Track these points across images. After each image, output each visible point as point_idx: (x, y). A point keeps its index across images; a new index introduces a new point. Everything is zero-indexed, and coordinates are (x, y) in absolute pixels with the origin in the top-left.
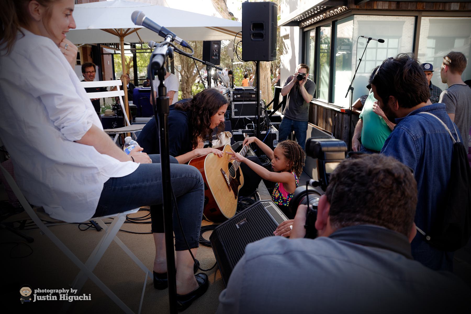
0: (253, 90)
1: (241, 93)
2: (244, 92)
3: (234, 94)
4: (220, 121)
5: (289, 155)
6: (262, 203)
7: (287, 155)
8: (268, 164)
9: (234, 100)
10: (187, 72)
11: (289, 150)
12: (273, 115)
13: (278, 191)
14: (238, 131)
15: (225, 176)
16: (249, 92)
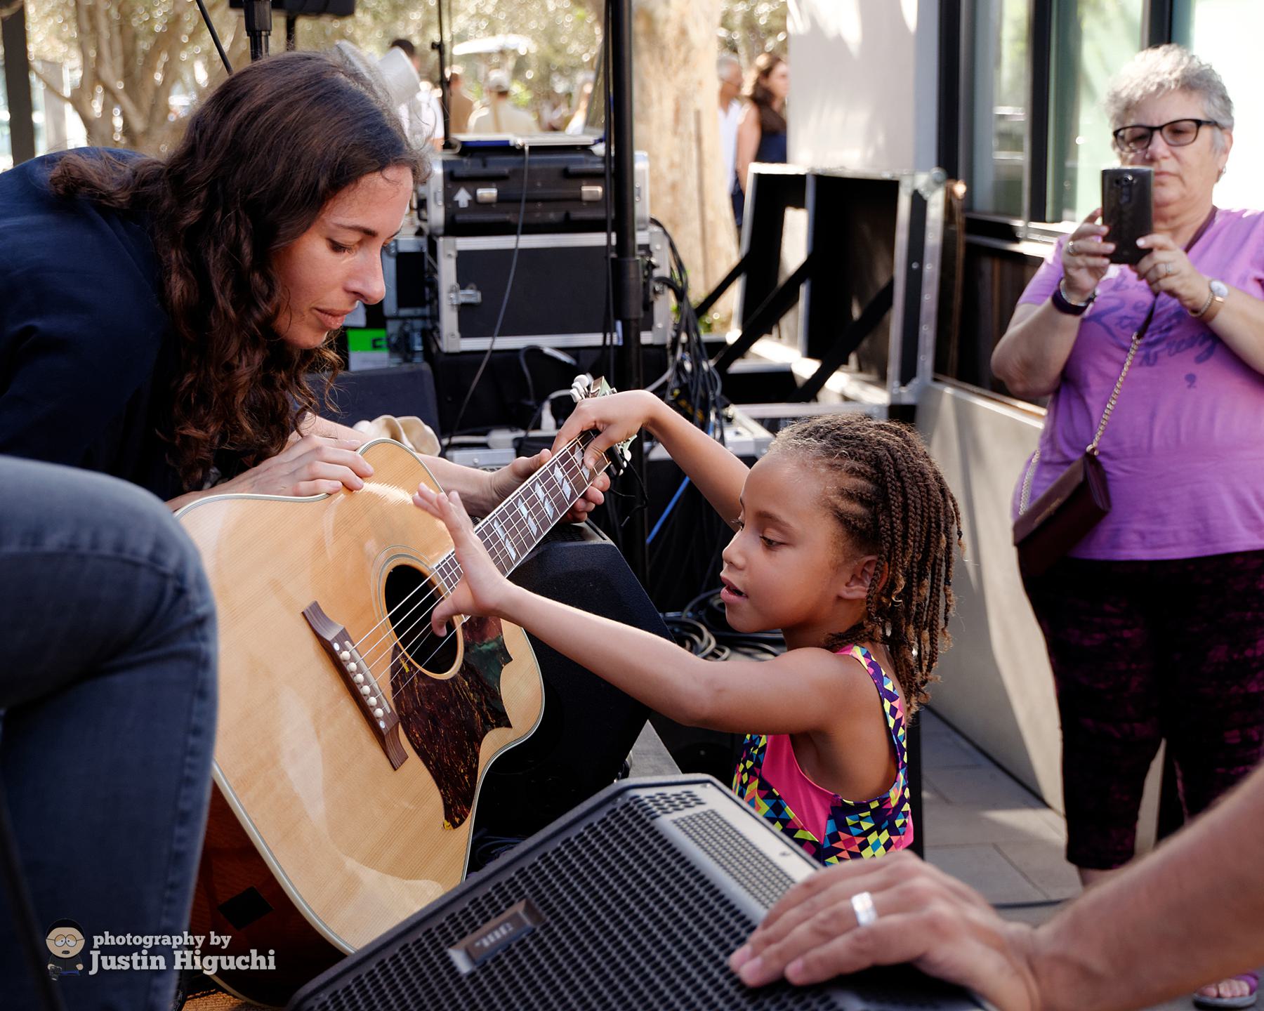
0: (585, 149)
1: (506, 170)
2: (523, 161)
3: (453, 179)
6: (643, 793)
9: (454, 227)
10: (124, 99)
12: (738, 366)
13: (756, 784)
14: (485, 446)
15: (345, 655)
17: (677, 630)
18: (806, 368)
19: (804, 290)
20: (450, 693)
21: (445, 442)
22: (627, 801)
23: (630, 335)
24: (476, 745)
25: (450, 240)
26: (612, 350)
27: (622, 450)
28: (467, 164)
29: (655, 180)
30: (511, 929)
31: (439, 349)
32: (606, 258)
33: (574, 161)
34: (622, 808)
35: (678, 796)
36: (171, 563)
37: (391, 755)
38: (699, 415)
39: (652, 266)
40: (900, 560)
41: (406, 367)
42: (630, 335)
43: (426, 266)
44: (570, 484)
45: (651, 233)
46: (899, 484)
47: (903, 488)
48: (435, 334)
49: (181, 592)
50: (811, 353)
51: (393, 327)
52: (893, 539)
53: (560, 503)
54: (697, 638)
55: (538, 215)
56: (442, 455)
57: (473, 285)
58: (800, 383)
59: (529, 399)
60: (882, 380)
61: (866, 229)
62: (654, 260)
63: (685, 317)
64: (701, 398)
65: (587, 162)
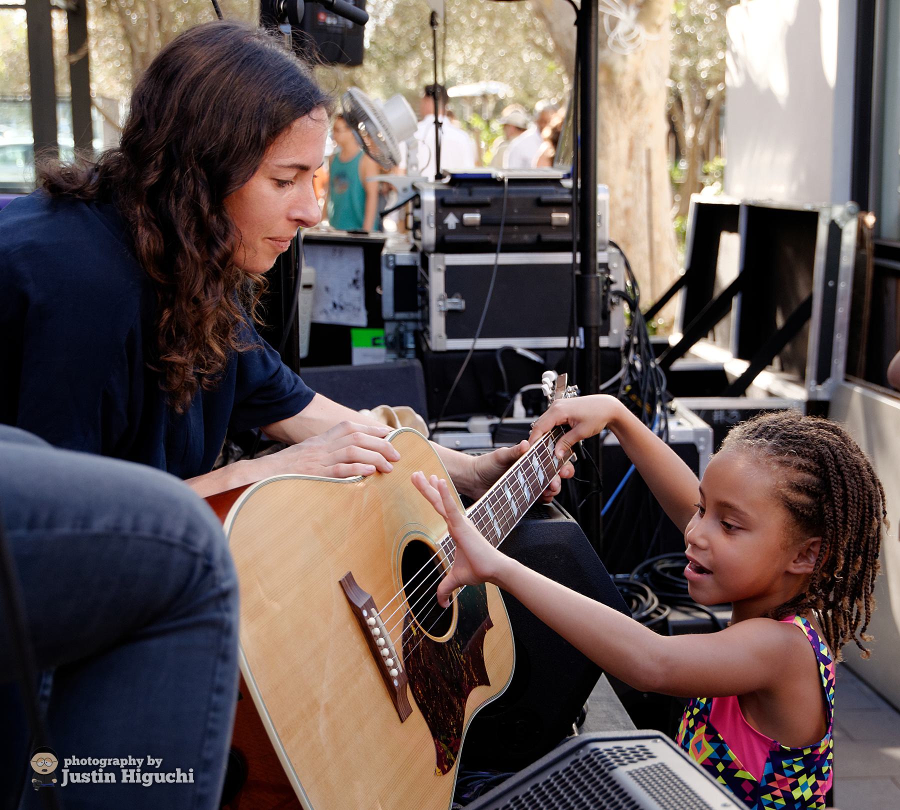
0: (556, 182)
1: (488, 199)
2: (503, 192)
3: (443, 205)
6: (602, 746)
9: (444, 245)
12: (679, 365)
13: (703, 729)
14: (465, 430)
15: (371, 621)
16: (532, 191)
17: (625, 590)
18: (737, 368)
19: (736, 302)
21: (432, 426)
23: (591, 339)
25: (440, 256)
26: (575, 352)
29: (612, 206)
31: (428, 347)
32: (572, 274)
33: (546, 192)
36: (201, 543)
37: (401, 711)
38: (647, 408)
39: (609, 282)
41: (402, 362)
42: (591, 339)
43: (419, 277)
45: (610, 254)
46: (839, 478)
48: (425, 335)
49: (208, 569)
50: (741, 354)
51: (390, 328)
52: (836, 525)
53: (535, 488)
54: (642, 598)
55: (514, 237)
56: (430, 438)
57: (459, 295)
58: (731, 381)
59: (503, 391)
60: (801, 380)
61: (789, 252)
62: (612, 277)
64: (649, 394)
65: (557, 192)
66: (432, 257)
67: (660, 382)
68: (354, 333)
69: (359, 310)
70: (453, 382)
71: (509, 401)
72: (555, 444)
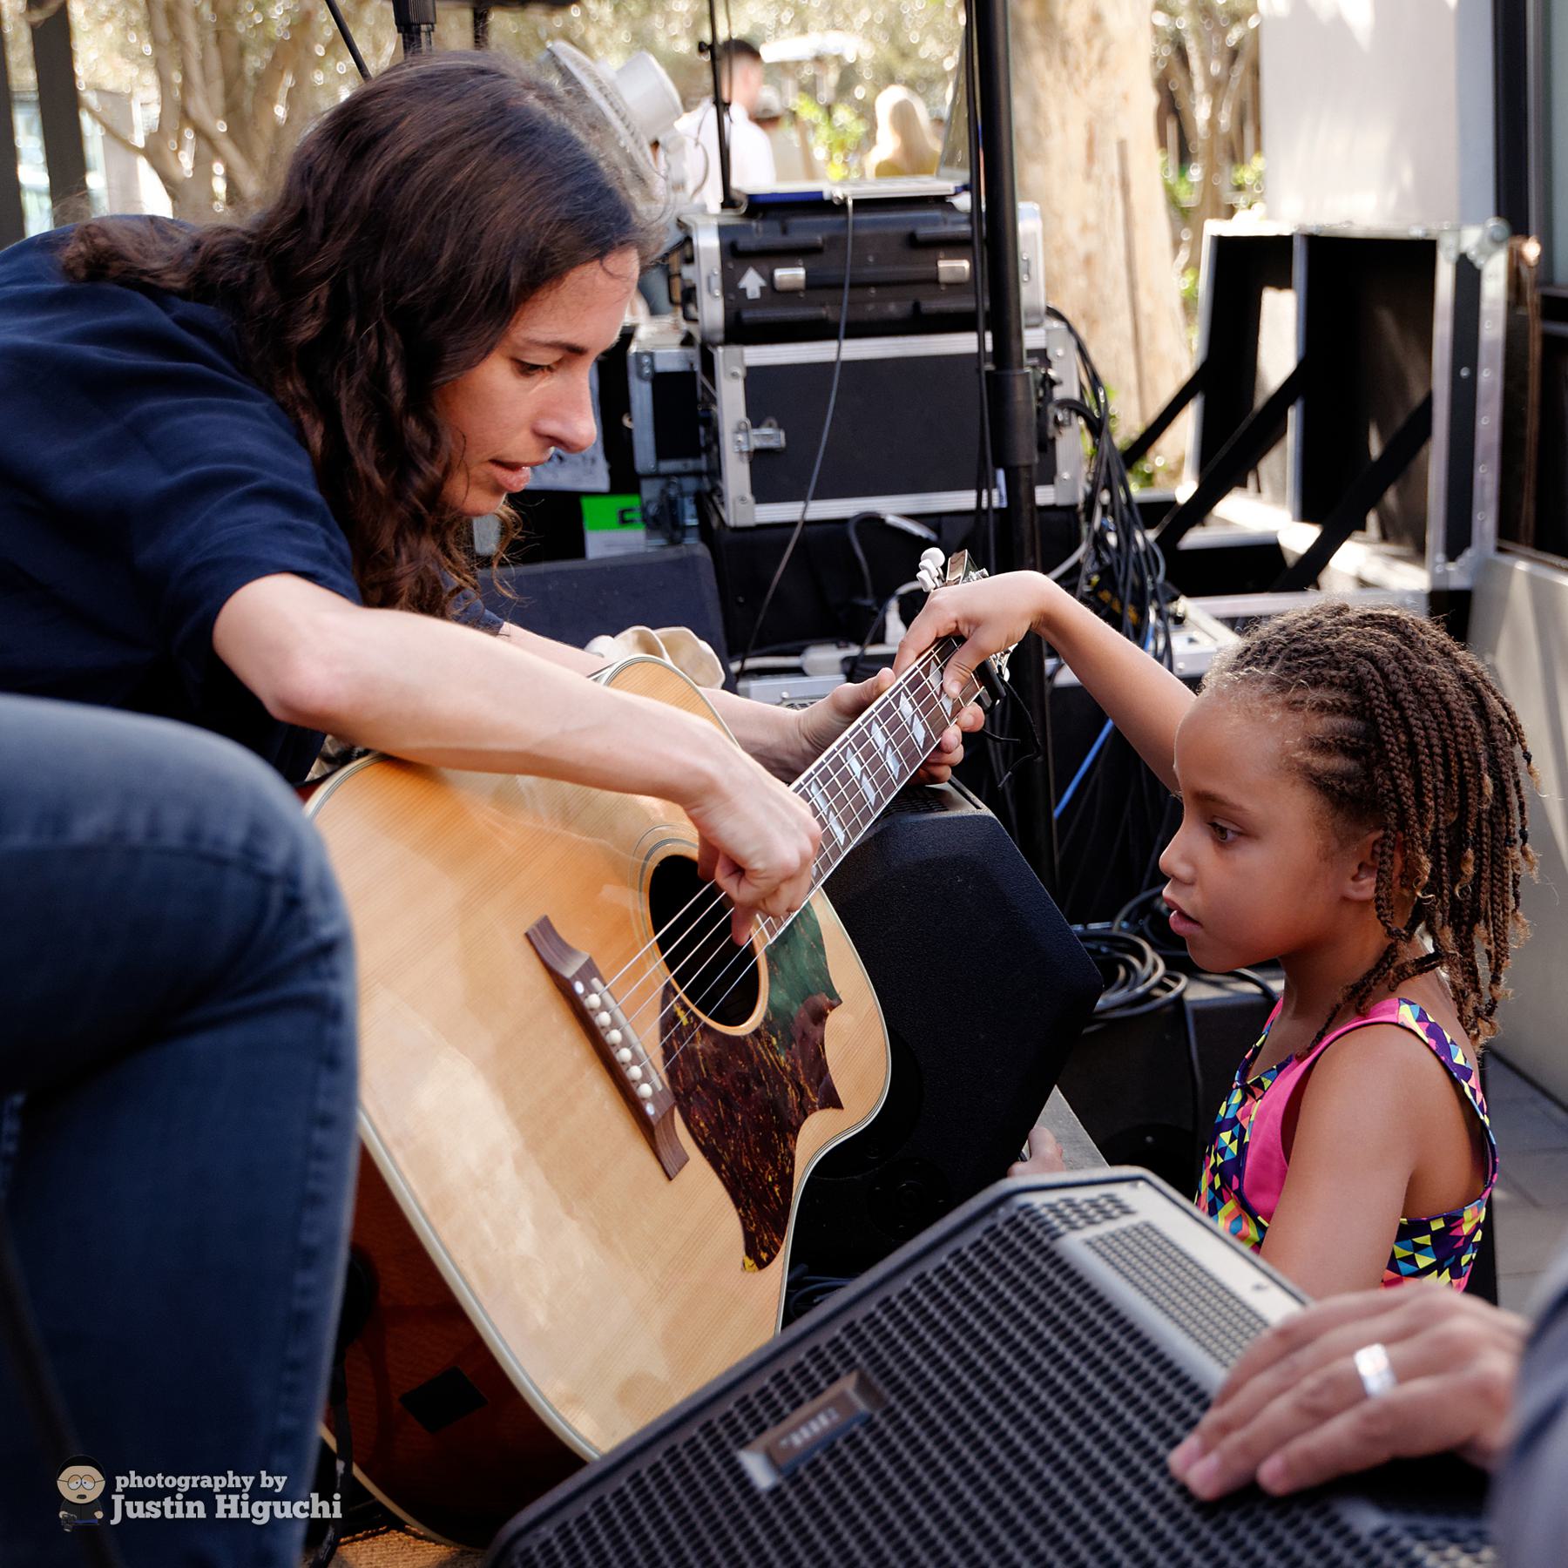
0: (940, 201)
3: (735, 254)
4: (538, 434)
5: (1369, 777)
6: (1038, 1200)
7: (1346, 777)
8: (1147, 997)
9: (740, 330)
10: (227, 147)
11: (1355, 724)
12: (1195, 538)
14: (798, 671)
15: (593, 1000)
18: (1299, 538)
19: (1293, 415)
20: (750, 1057)
21: (735, 667)
22: (1014, 1211)
23: (1019, 491)
24: (790, 1137)
25: (735, 350)
26: (991, 512)
27: (1000, 667)
28: (757, 230)
30: (835, 1417)
32: (979, 370)
33: (925, 222)
34: (1007, 1223)
35: (1093, 1203)
36: (277, 856)
37: (664, 1159)
38: (1131, 614)
39: (1049, 383)
40: (1418, 834)
41: (671, 553)
42: (1019, 491)
44: (924, 724)
47: (1404, 718)
48: (715, 498)
49: (294, 902)
50: (1307, 513)
51: (650, 490)
53: (909, 752)
58: (1291, 561)
59: (865, 596)
60: (1418, 553)
62: (1052, 373)
63: (1105, 460)
64: (1133, 586)
65: (945, 222)
66: (720, 353)
67: (1153, 565)
68: (586, 503)
69: (593, 461)
70: (770, 585)
71: (876, 614)
72: (942, 670)
